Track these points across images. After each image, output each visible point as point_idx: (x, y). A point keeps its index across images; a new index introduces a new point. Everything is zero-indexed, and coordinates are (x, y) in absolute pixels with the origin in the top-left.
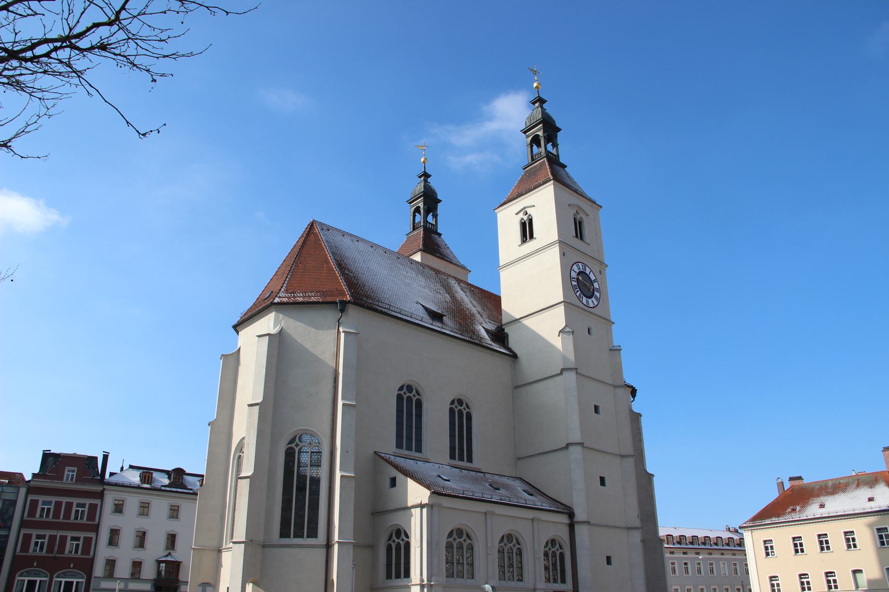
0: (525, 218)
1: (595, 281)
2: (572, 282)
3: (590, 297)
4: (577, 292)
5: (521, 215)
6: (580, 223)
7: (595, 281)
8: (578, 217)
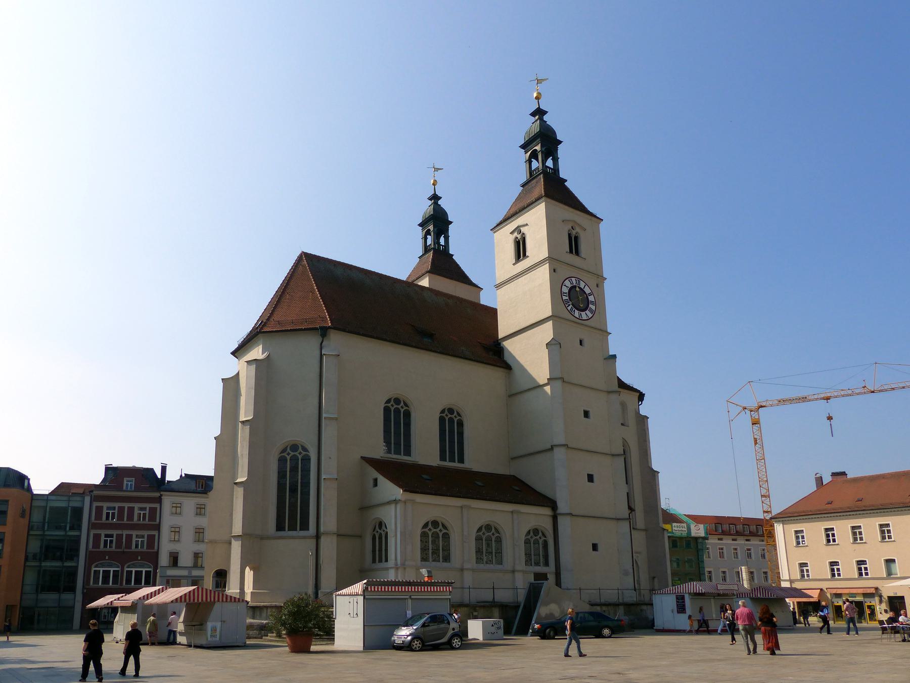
0: (519, 236)
1: (590, 294)
2: (563, 297)
3: (584, 310)
4: (568, 306)
5: (516, 234)
6: (576, 238)
7: (590, 294)
8: (574, 233)
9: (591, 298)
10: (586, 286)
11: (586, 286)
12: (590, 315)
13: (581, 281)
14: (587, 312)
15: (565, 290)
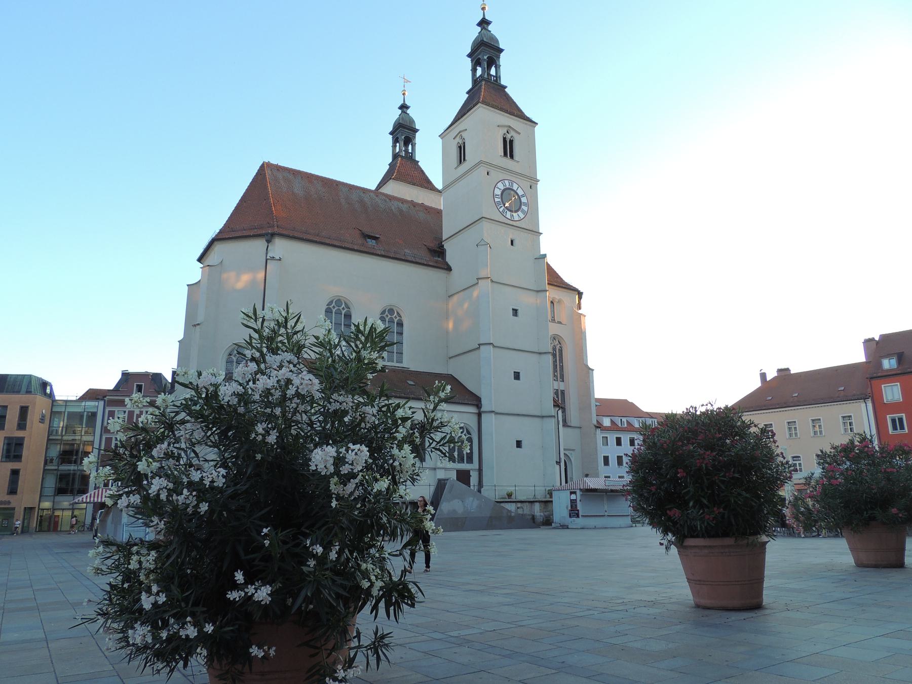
1: (523, 196)
2: (495, 198)
6: (511, 142)
7: (523, 196)
9: (524, 200)
10: (519, 188)
11: (519, 188)
12: (522, 216)
13: (514, 183)
14: (519, 213)
15: (498, 192)
